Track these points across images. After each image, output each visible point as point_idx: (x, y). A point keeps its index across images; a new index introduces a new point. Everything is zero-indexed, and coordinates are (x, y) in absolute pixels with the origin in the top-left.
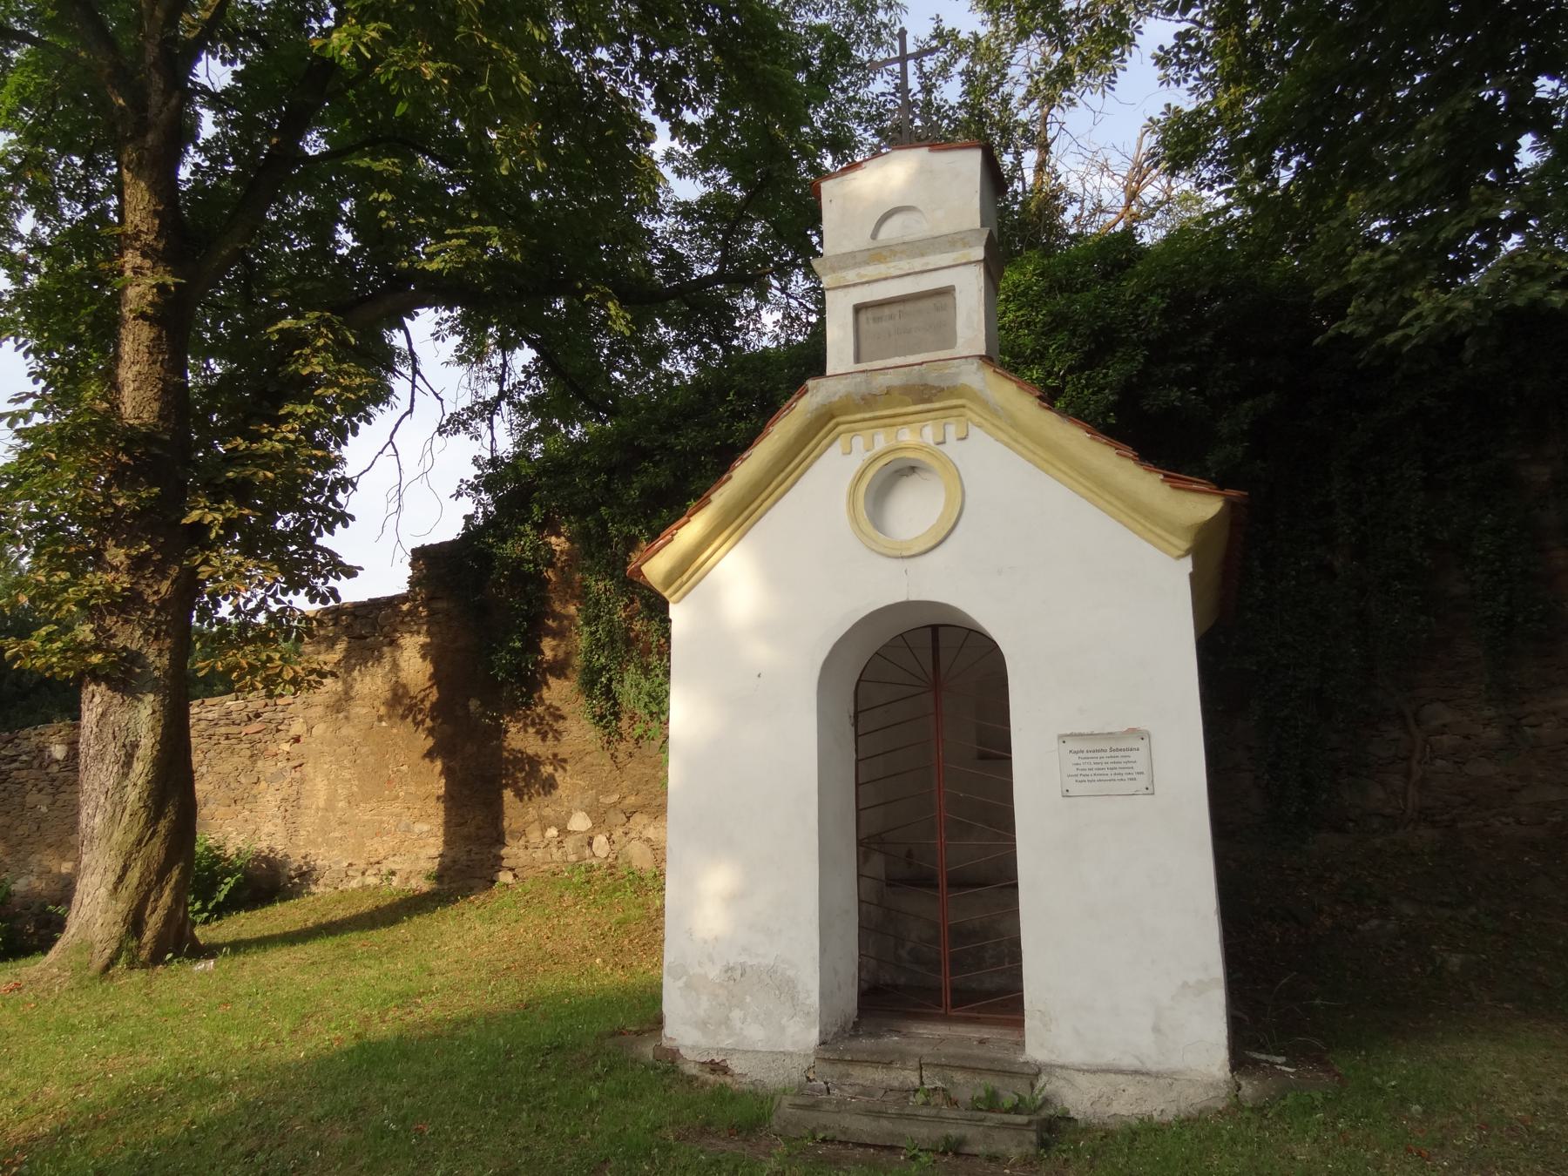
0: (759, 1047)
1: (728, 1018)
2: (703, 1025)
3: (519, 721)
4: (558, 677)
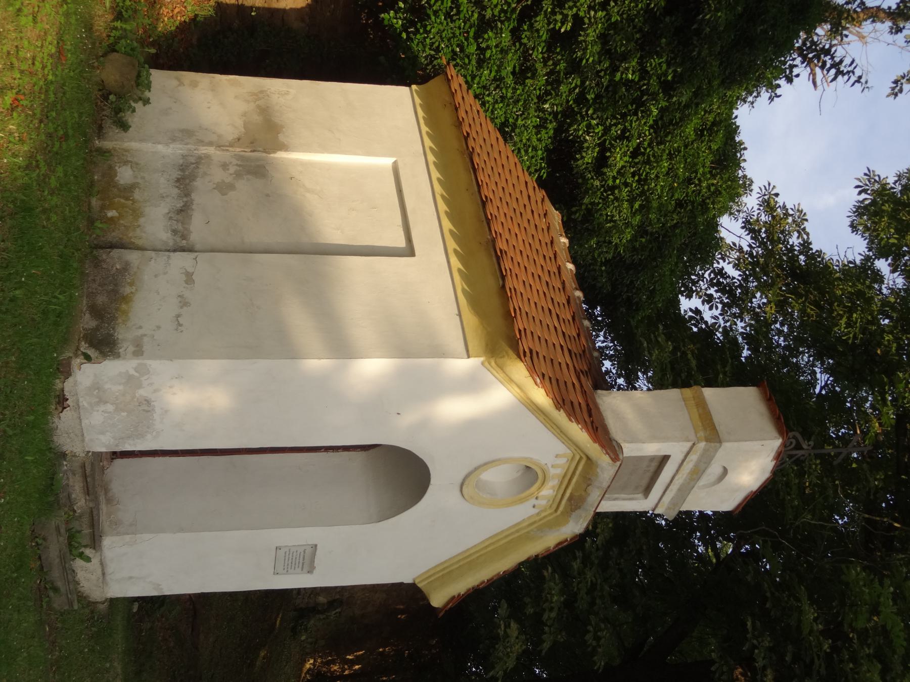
0: (85, 422)
1: (106, 402)
2: (96, 386)
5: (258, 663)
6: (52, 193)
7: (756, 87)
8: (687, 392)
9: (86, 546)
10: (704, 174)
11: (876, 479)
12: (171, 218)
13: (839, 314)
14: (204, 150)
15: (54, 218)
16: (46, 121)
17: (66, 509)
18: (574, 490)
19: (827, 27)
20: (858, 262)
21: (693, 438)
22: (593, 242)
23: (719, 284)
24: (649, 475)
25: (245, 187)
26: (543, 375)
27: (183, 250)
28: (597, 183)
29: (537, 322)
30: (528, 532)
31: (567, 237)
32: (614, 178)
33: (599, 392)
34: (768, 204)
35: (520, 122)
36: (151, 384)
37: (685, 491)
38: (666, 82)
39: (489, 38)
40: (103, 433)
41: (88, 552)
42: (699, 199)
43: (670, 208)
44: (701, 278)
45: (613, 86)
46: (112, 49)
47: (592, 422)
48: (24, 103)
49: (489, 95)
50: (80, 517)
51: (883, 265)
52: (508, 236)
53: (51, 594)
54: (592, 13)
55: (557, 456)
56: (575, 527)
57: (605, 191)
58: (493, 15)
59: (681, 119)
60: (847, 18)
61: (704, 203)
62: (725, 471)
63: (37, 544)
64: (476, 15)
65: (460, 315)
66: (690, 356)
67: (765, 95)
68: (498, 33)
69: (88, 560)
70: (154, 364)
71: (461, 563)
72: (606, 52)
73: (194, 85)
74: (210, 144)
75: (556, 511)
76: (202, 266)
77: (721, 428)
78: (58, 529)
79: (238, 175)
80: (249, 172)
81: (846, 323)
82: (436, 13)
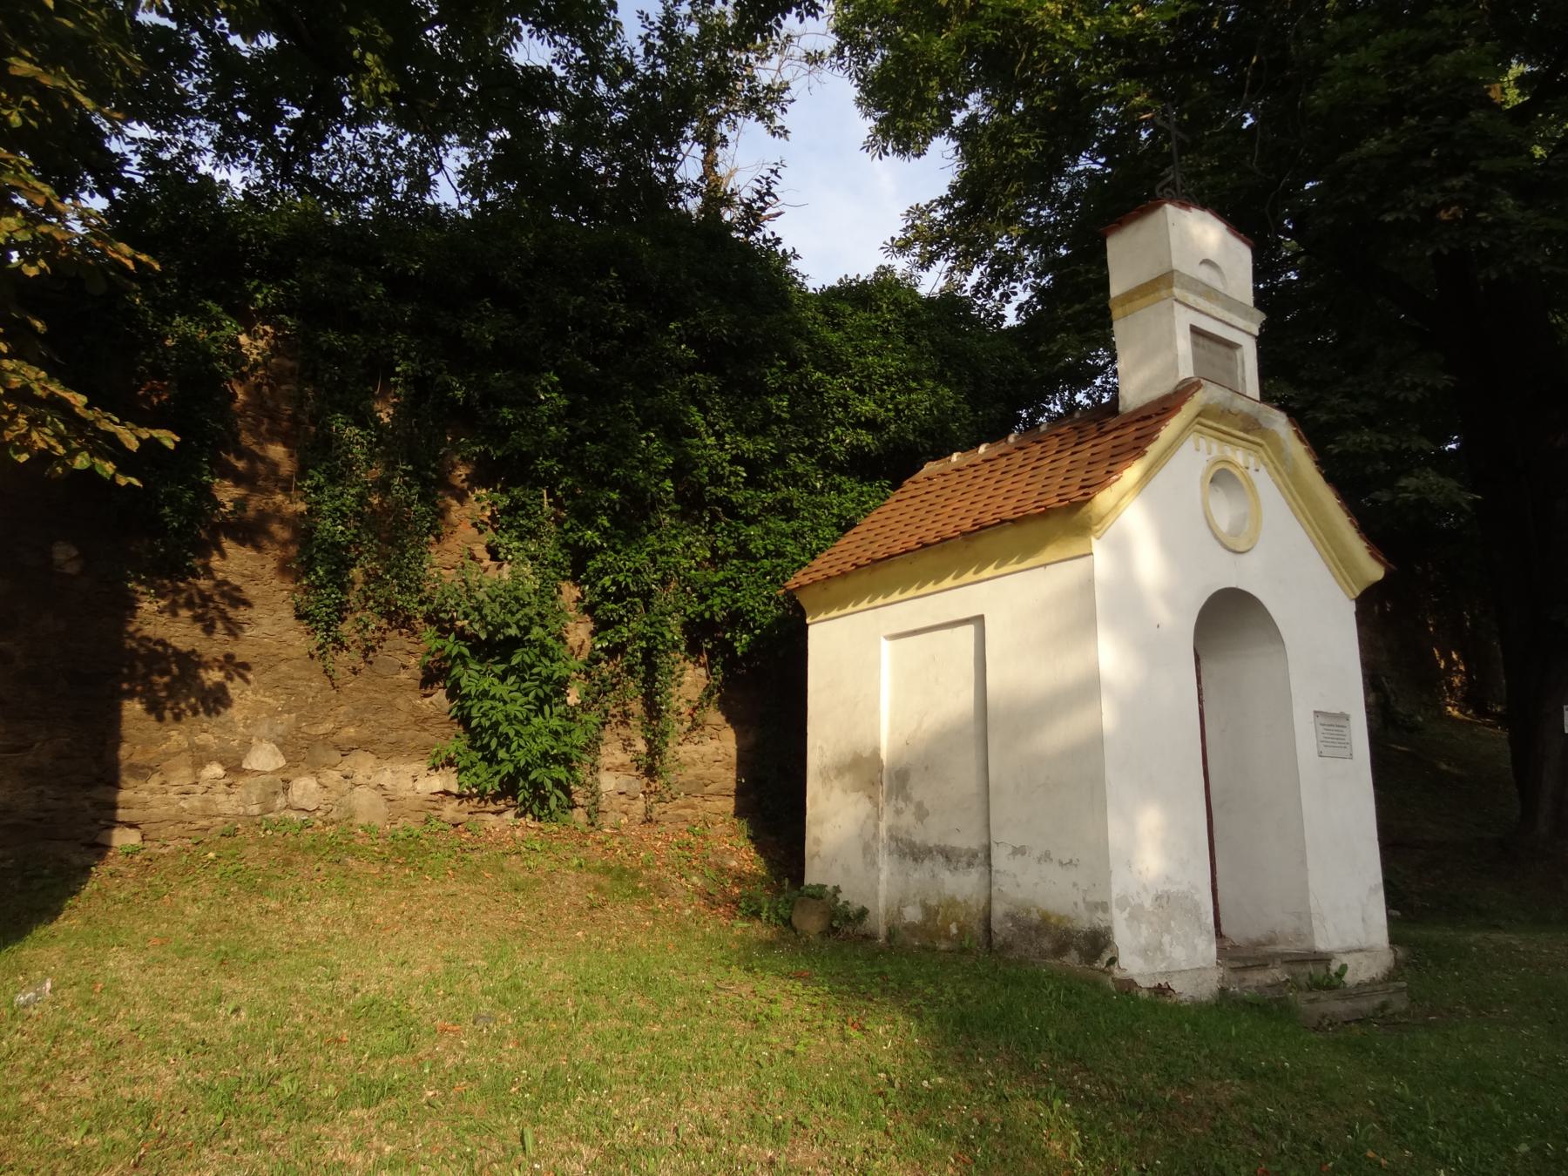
0: (1184, 966)
2: (1144, 952)
3: (163, 597)
4: (242, 542)
5: (1456, 771)
6: (942, 992)
7: (787, 274)
8: (1116, 313)
9: (1328, 970)
10: (877, 318)
11: (1201, 91)
12: (956, 869)
13: (1016, 158)
14: (883, 833)
15: (967, 991)
16: (869, 995)
17: (1285, 990)
18: (1235, 427)
19: (723, 210)
20: (957, 144)
21: (1169, 300)
22: (954, 427)
23: (989, 289)
24: (1214, 346)
25: (918, 792)
26: (1108, 472)
27: (988, 856)
28: (893, 427)
29: (1049, 481)
30: (1288, 475)
31: (951, 454)
32: (887, 410)
33: (1120, 409)
34: (902, 247)
35: (836, 511)
36: (1138, 893)
37: (1230, 304)
38: (788, 366)
39: (756, 547)
40: (1195, 948)
41: (1335, 967)
42: (903, 320)
43: (914, 349)
44: (982, 307)
45: (795, 419)
46: (788, 922)
47: (1157, 414)
48: (855, 1017)
49: (811, 544)
50: (1293, 974)
51: (958, 119)
52: (957, 519)
53: (1390, 1011)
54: (727, 446)
55: (1198, 450)
56: (1280, 423)
57: (901, 419)
58: (734, 544)
59: (824, 347)
60: (716, 192)
61: (909, 315)
62: (1206, 262)
63: (1330, 1025)
64: (735, 562)
65: (1045, 565)
66: (1070, 312)
67: (794, 264)
68: (750, 538)
69: (1344, 968)
70: (1116, 891)
71: (1329, 547)
72: (762, 430)
73: (817, 841)
74: (876, 826)
75: (1261, 446)
76: (1006, 838)
77: (1156, 272)
78: (1311, 1001)
79: (907, 798)
80: (904, 787)
81: (1025, 148)
82: (735, 601)
